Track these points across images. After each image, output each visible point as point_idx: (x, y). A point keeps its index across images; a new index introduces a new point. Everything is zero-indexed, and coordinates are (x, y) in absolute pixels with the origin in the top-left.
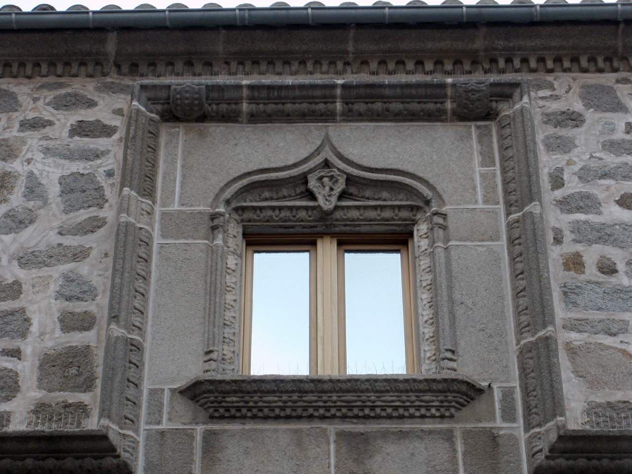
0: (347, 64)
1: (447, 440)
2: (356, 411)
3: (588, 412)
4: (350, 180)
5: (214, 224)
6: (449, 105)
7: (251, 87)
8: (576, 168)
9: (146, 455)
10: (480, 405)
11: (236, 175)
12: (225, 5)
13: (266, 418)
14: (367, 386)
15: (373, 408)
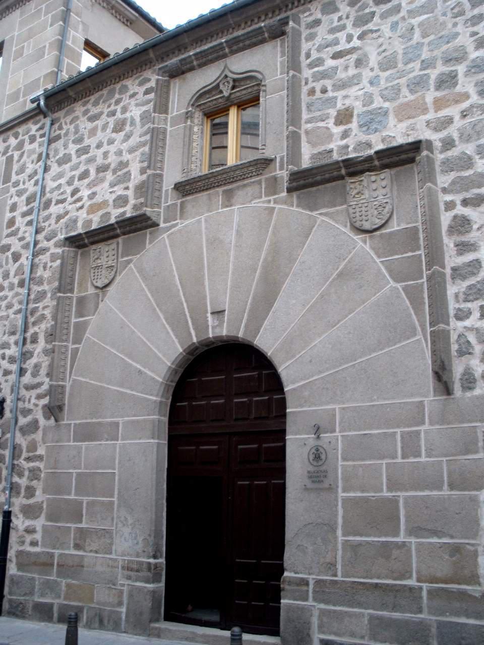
0: (233, 29)
1: (232, 192)
2: (228, 180)
3: (311, 158)
4: (235, 80)
5: (188, 116)
6: (266, 35)
7: (194, 55)
8: (316, 47)
9: (164, 216)
10: (271, 166)
11: (195, 93)
12: (182, 23)
13: (200, 191)
14: (229, 170)
15: (233, 178)
